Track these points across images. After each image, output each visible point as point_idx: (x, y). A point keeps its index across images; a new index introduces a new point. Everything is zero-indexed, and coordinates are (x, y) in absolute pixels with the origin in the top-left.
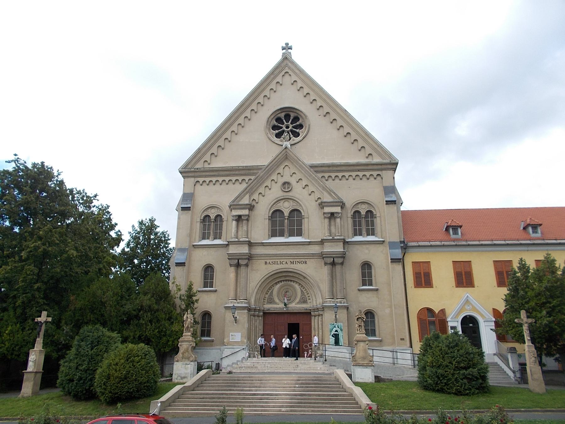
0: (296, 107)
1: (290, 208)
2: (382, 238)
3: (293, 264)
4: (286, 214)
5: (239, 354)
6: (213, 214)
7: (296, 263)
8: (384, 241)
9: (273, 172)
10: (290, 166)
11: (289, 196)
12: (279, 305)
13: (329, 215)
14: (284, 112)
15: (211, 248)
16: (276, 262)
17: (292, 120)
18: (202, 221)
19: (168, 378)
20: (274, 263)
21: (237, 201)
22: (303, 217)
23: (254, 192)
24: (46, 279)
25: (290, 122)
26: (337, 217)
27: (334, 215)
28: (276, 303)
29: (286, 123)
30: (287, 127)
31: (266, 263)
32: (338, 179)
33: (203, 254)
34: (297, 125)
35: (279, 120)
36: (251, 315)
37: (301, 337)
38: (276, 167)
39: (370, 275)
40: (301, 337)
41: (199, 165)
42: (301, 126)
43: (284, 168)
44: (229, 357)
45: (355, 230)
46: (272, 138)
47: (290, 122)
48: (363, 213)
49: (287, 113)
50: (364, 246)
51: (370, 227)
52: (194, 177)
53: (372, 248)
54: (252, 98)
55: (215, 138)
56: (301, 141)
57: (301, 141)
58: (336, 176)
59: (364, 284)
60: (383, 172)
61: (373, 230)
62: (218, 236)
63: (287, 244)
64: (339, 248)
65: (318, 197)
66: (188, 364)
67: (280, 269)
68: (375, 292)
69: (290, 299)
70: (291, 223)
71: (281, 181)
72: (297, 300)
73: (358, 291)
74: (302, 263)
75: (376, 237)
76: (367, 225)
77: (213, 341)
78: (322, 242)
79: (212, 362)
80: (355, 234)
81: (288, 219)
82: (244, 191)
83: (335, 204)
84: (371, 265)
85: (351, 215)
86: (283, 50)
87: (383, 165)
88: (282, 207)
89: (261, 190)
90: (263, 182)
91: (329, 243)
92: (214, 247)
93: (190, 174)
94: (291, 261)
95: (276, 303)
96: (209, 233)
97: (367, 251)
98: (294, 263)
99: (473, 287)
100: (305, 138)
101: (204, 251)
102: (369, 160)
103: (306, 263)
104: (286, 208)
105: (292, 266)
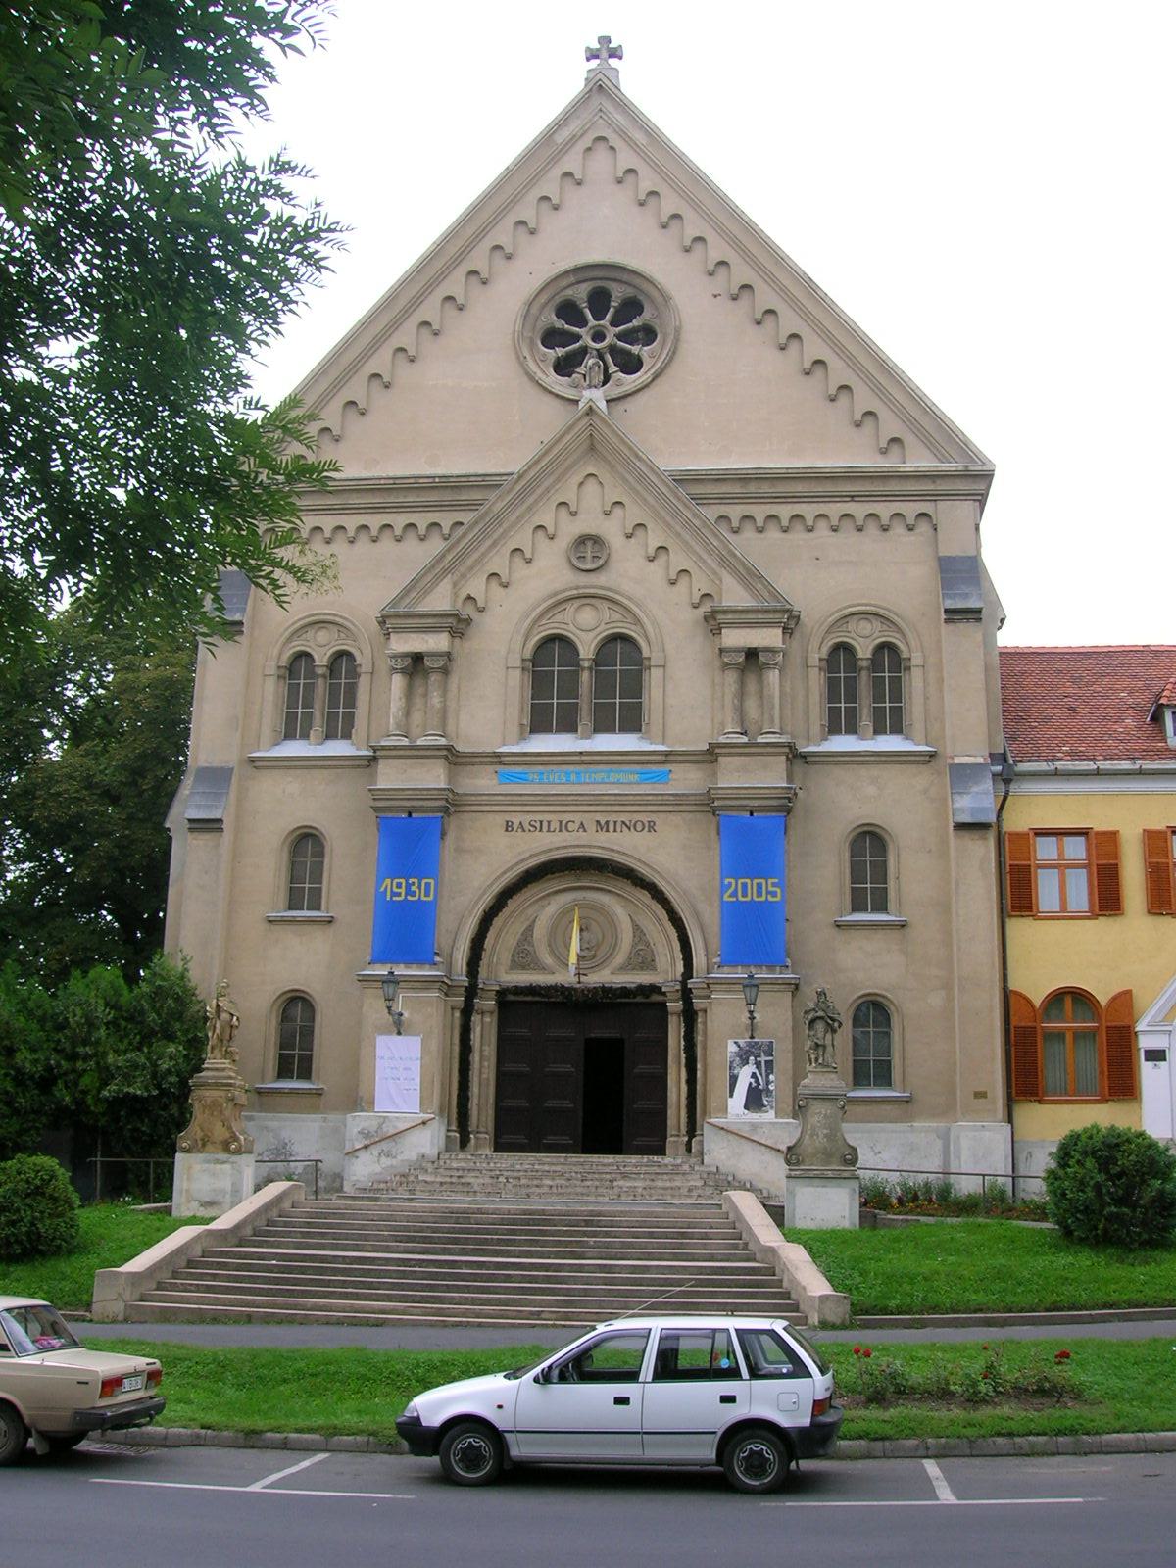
0: (633, 263)
2: (927, 745)
3: (607, 831)
4: (587, 649)
16: (545, 825)
17: (618, 311)
20: (538, 825)
25: (590, 316)
29: (592, 322)
31: (508, 827)
34: (635, 330)
36: (453, 1009)
39: (881, 873)
43: (581, 484)
45: (834, 713)
47: (608, 316)
50: (863, 771)
59: (858, 906)
61: (897, 713)
62: (339, 726)
66: (224, 1163)
67: (557, 848)
68: (895, 934)
69: (594, 956)
71: (571, 529)
72: (620, 958)
73: (267, 926)
74: (639, 828)
76: (878, 697)
78: (712, 754)
80: (834, 729)
85: (279, 667)
88: (572, 627)
89: (498, 562)
94: (598, 822)
96: (308, 717)
98: (611, 828)
103: (651, 827)
104: (587, 630)
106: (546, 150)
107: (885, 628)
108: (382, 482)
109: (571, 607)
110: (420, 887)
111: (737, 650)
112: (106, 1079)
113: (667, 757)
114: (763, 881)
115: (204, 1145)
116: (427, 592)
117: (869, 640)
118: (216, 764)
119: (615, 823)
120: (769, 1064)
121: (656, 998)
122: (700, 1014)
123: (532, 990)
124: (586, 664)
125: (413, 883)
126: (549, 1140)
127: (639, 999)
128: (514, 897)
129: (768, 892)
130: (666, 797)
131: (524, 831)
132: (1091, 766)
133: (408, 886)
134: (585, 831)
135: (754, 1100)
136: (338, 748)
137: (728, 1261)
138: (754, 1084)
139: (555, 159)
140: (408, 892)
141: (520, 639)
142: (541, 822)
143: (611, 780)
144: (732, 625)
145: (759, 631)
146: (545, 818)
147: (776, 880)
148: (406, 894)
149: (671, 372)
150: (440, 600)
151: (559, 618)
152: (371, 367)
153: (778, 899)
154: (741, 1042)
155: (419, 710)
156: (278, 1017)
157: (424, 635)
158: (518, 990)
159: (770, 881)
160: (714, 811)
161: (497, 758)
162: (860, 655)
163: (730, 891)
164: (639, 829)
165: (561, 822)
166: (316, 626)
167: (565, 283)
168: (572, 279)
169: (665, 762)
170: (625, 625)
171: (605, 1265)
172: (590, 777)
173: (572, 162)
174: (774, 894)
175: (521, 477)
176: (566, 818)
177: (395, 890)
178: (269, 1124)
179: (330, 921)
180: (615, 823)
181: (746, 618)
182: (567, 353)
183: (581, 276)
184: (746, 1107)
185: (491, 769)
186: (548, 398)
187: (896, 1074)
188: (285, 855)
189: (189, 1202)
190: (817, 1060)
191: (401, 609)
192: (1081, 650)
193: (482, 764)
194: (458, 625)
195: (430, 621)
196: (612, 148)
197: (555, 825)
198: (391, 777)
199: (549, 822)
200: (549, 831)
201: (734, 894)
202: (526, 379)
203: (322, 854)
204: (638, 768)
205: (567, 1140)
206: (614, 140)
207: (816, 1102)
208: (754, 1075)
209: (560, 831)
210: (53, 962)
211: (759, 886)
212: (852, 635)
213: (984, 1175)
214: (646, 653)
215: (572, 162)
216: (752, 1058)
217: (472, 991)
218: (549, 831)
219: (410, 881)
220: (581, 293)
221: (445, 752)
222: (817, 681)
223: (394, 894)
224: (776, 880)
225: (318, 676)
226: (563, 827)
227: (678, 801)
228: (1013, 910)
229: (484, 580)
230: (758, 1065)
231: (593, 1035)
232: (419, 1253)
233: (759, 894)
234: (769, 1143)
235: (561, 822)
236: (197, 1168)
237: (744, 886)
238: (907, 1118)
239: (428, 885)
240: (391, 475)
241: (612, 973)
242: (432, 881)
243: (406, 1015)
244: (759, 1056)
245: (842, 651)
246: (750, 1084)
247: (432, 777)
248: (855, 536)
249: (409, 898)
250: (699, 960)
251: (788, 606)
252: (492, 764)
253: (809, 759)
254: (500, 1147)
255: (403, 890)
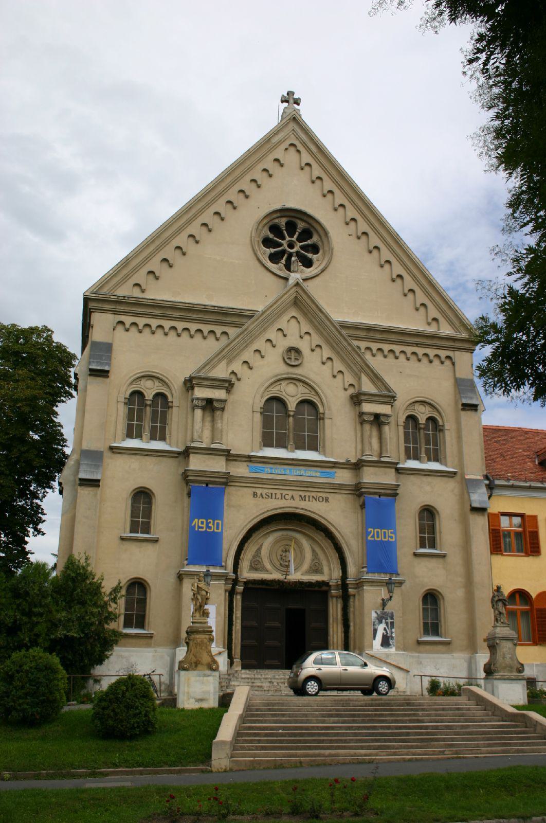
0: (310, 211)
2: (177, 448)
3: (305, 500)
4: (292, 405)
6: (150, 389)
8: (455, 473)
9: (270, 324)
10: (301, 318)
11: (296, 374)
12: (271, 574)
13: (204, 403)
15: (146, 457)
17: (300, 234)
18: (127, 401)
19: (324, 713)
20: (270, 495)
21: (203, 371)
22: (170, 404)
23: (235, 357)
25: (295, 236)
26: (218, 409)
27: (213, 402)
28: (267, 571)
29: (294, 239)
30: (291, 246)
31: (255, 495)
32: (382, 355)
33: (130, 467)
34: (308, 246)
35: (274, 229)
38: (276, 316)
41: (125, 291)
42: (315, 249)
43: (288, 321)
45: (407, 450)
46: (264, 262)
47: (295, 236)
48: (149, 395)
49: (291, 219)
50: (424, 479)
52: (115, 312)
53: (437, 482)
54: (229, 180)
55: (158, 243)
56: (317, 276)
57: (317, 276)
58: (186, 329)
59: (423, 545)
60: (456, 352)
61: (163, 429)
62: (159, 433)
63: (294, 462)
64: (387, 478)
65: (350, 383)
66: (209, 676)
68: (441, 560)
70: (299, 425)
71: (283, 344)
72: (306, 566)
74: (321, 499)
75: (441, 464)
76: (154, 420)
77: (152, 637)
78: (357, 466)
79: (160, 675)
80: (408, 457)
81: (293, 416)
82: (218, 355)
83: (381, 399)
84: (436, 513)
85: (125, 398)
86: (282, 102)
87: (456, 342)
88: (284, 394)
89: (248, 355)
90: (252, 342)
91: (372, 468)
92: (152, 456)
93: (107, 306)
94: (300, 496)
95: (268, 571)
96: (140, 427)
97: (428, 488)
98: (307, 499)
99: (491, 553)
100: (325, 272)
101: (133, 460)
102: (432, 329)
103: (327, 500)
104: (292, 395)
105: (303, 504)
106: (266, 144)
107: (431, 409)
108: (187, 305)
109: (284, 383)
110: (213, 524)
111: (203, 399)
112: (54, 625)
113: (335, 465)
114: (386, 531)
115: (196, 666)
116: (214, 367)
117: (152, 390)
118: (93, 448)
119: (309, 496)
120: (392, 623)
121: (324, 588)
122: (352, 597)
123: (263, 582)
124: (292, 413)
125: (210, 522)
126: (268, 662)
127: (316, 588)
128: (256, 532)
129: (389, 537)
131: (263, 498)
132: (527, 484)
133: (207, 524)
134: (294, 500)
135: (386, 642)
136: (157, 445)
137: (490, 722)
138: (385, 634)
139: (270, 151)
140: (208, 527)
141: (258, 396)
142: (272, 494)
143: (307, 475)
144: (199, 385)
145: (380, 405)
146: (274, 491)
147: (392, 531)
148: (206, 528)
149: (329, 269)
150: (221, 372)
151: (278, 388)
152: (175, 243)
153: (393, 540)
154: (379, 612)
155: (207, 429)
157: (212, 389)
158: (254, 582)
159: (390, 531)
160: (360, 495)
161: (249, 458)
162: (420, 422)
163: (371, 535)
165: (282, 494)
166: (147, 378)
167: (275, 216)
168: (278, 215)
169: (333, 467)
170: (311, 396)
171: (448, 725)
172: (296, 472)
173: (279, 153)
174: (392, 537)
175: (263, 313)
177: (200, 525)
178: (123, 654)
179: (156, 541)
180: (309, 496)
181: (372, 398)
182: (275, 251)
183: (283, 214)
184: (382, 645)
185: (245, 464)
186: (269, 274)
187: (442, 629)
188: (130, 502)
189: (189, 699)
190: (500, 620)
191: (202, 374)
192: (491, 428)
193: (241, 461)
194: (228, 385)
195: (216, 383)
196: (298, 151)
197: (279, 496)
198: (196, 463)
199: (276, 494)
200: (276, 498)
201: (373, 536)
202: (257, 262)
203: (150, 503)
204: (319, 469)
205: (276, 662)
206: (300, 147)
207: (504, 641)
208: (385, 629)
209: (282, 499)
211: (385, 533)
212: (416, 411)
213: (421, 676)
214: (170, 399)
215: (279, 153)
216: (384, 620)
217: (235, 582)
218: (276, 498)
219: (209, 521)
221: (226, 453)
223: (199, 527)
224: (392, 531)
225: (146, 405)
226: (283, 497)
227: (341, 487)
228: (531, 552)
229: (241, 364)
230: (387, 623)
231: (290, 607)
232: (342, 723)
233: (385, 537)
234: (394, 663)
236: (193, 679)
237: (378, 532)
238: (450, 652)
239: (218, 523)
240: (191, 302)
241: (302, 575)
242: (220, 522)
244: (387, 619)
245: (412, 418)
246: (383, 633)
247: (218, 465)
248: (417, 364)
249: (208, 530)
250: (352, 570)
252: (245, 461)
253: (114, 450)
254: (244, 667)
255: (204, 526)
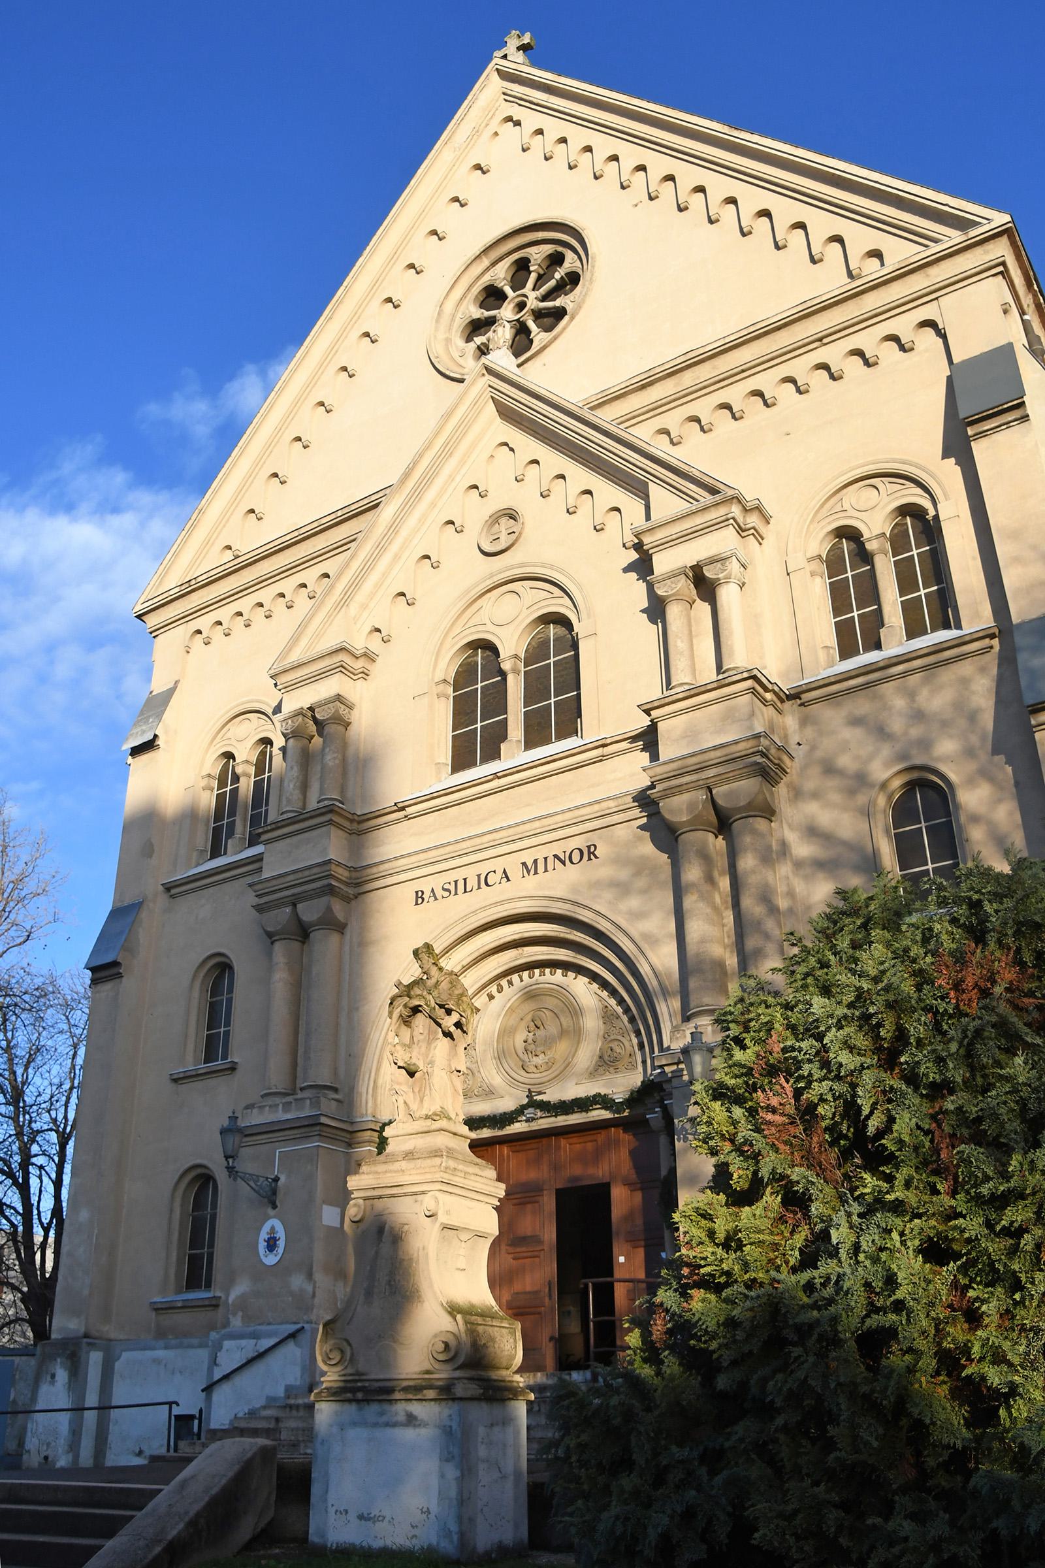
1: (520, 618)
3: (536, 873)
5: (274, 1361)
7: (550, 867)
14: (501, 259)
20: (452, 888)
24: (10, 1193)
37: (622, 1259)
40: (622, 1259)
44: (237, 1380)
51: (855, 614)
72: (586, 1055)
73: (173, 1085)
92: (225, 881)
130: (604, 805)
156: (183, 1205)
164: (577, 853)
165: (479, 876)
168: (486, 262)
176: (483, 869)
191: (295, 656)
209: (479, 888)
210: (698, 1294)
220: (501, 274)
222: (817, 592)
235: (479, 876)
243: (283, 1179)
251: (730, 492)
253: (805, 697)
